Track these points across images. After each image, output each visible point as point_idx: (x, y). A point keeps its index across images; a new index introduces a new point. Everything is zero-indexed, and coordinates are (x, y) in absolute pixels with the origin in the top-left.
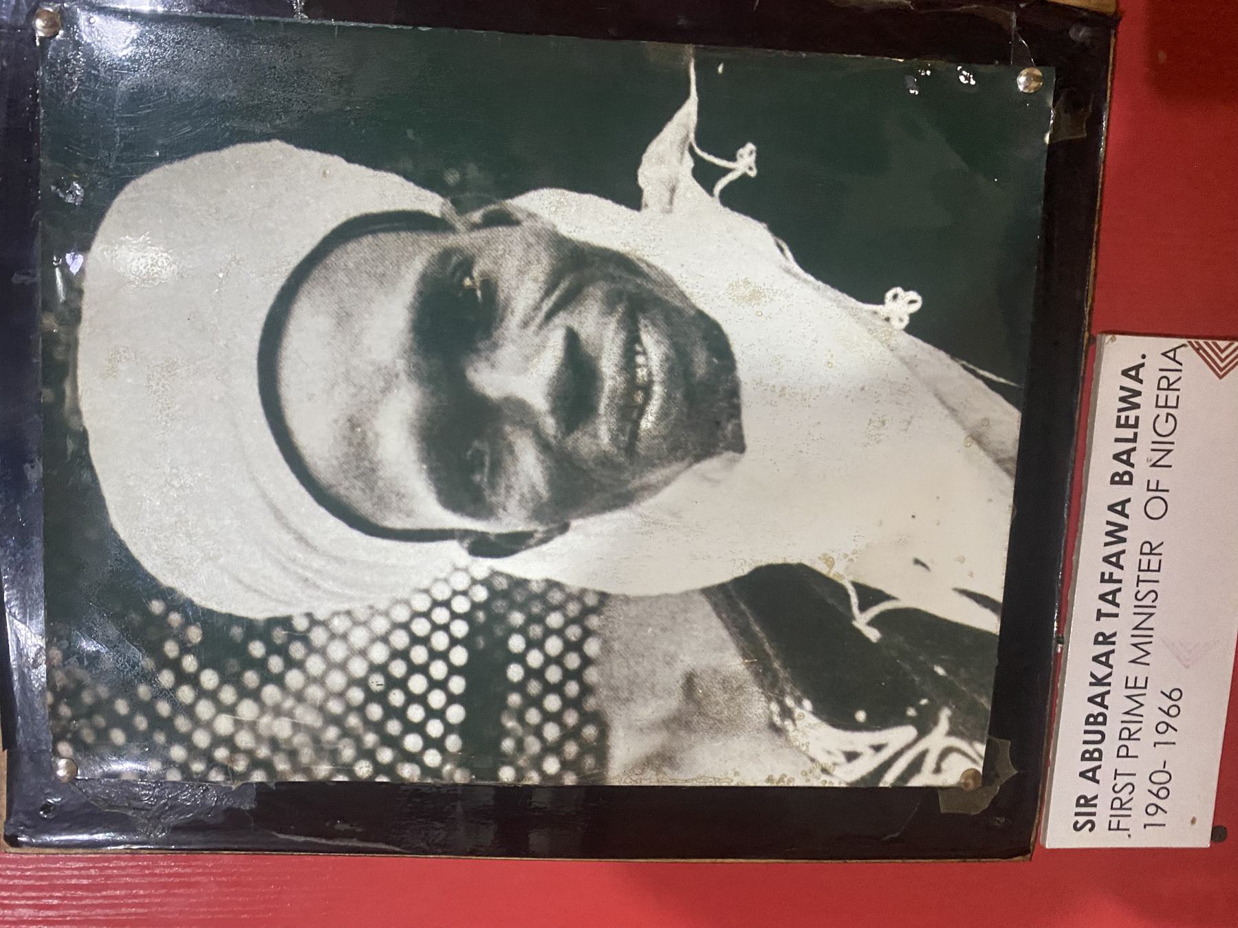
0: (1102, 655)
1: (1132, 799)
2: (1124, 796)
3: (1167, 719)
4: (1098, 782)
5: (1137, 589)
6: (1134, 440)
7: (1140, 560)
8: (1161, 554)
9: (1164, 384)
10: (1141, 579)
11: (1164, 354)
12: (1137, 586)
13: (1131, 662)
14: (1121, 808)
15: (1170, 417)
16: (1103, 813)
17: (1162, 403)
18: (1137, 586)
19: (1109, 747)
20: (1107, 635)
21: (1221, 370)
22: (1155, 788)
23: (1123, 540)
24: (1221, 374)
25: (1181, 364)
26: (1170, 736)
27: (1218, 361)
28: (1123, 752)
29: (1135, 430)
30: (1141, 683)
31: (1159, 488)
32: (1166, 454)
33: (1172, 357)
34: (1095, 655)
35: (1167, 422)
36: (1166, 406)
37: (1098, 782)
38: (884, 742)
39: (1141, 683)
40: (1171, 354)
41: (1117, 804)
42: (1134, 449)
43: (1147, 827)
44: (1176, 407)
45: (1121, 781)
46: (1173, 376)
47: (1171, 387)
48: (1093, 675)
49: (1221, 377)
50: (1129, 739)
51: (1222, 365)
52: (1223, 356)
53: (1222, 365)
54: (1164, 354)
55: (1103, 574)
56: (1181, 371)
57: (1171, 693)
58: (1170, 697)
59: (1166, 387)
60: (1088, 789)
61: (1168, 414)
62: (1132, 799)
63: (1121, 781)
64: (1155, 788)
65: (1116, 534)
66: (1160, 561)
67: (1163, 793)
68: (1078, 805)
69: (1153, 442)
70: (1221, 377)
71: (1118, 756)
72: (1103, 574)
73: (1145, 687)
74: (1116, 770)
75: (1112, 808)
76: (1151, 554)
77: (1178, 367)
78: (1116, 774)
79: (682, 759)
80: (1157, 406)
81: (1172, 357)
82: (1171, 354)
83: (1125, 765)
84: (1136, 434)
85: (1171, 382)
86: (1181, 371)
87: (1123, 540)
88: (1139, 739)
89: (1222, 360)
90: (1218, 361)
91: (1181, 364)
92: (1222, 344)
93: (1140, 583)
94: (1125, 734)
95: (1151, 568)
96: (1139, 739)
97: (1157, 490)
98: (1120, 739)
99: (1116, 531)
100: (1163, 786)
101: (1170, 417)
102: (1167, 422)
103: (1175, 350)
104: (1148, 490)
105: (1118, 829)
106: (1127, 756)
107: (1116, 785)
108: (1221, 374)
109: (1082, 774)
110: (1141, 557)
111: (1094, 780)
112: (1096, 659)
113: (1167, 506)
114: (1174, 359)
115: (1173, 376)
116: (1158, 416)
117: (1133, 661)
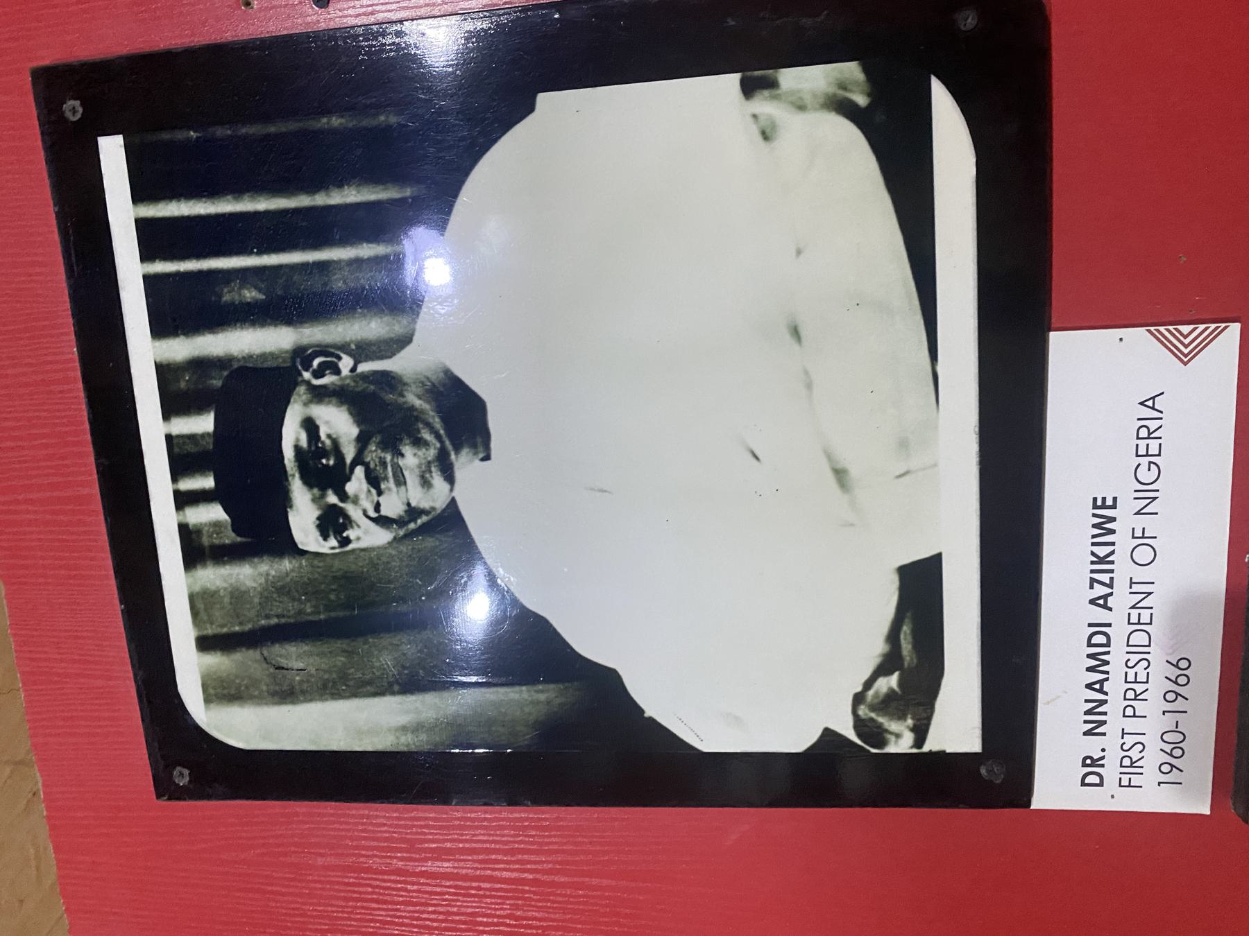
0: (1095, 683)
1: (1143, 757)
2: (1135, 754)
3: (1175, 688)
4: (1110, 609)
5: (1123, 741)
6: (1108, 645)
7: (1137, 445)
8: (1160, 438)
9: (1144, 432)
10: (1133, 581)
11: (1142, 404)
12: (1123, 738)
13: (1135, 514)
14: (1131, 766)
15: (1152, 465)
16: (1111, 771)
17: (1142, 451)
18: (1123, 738)
19: (1114, 706)
20: (1095, 758)
21: (1186, 356)
22: (1168, 748)
23: (1112, 532)
24: (1186, 360)
25: (1161, 412)
26: (1180, 704)
27: (1181, 338)
28: (1129, 712)
29: (1111, 575)
30: (1109, 502)
31: (1141, 622)
32: (1153, 501)
33: (1151, 405)
34: (1092, 598)
35: (1149, 470)
36: (1147, 455)
37: (1110, 609)
38: (803, 340)
39: (1109, 502)
40: (1150, 403)
41: (1127, 762)
42: (1111, 594)
43: (1161, 785)
44: (1151, 624)
45: (1129, 740)
46: (1153, 425)
47: (1134, 765)
48: (1093, 554)
49: (1185, 364)
50: (1135, 699)
51: (1186, 351)
52: (1186, 341)
53: (1186, 351)
54: (1142, 404)
55: (1095, 500)
56: (1161, 419)
57: (1177, 663)
58: (1177, 666)
59: (1146, 436)
60: (1093, 747)
61: (1150, 463)
62: (1143, 757)
63: (1129, 740)
64: (1168, 748)
65: (1098, 663)
66: (1152, 614)
67: (1178, 752)
68: (1084, 765)
69: (1135, 491)
70: (1185, 364)
71: (1124, 716)
72: (1095, 500)
73: (1149, 646)
74: (1123, 729)
75: (1121, 766)
76: (1148, 438)
77: (1159, 415)
78: (1123, 733)
79: (363, 248)
80: (1137, 455)
81: (1151, 405)
82: (1150, 403)
83: (1131, 724)
84: (1112, 579)
85: (1151, 431)
86: (1161, 419)
87: (1112, 532)
88: (1104, 734)
89: (1186, 346)
90: (1181, 338)
91: (1161, 412)
92: (1185, 329)
93: (1133, 585)
94: (1131, 695)
95: (1137, 714)
96: (1104, 734)
97: (1143, 537)
98: (1125, 699)
99: (1103, 523)
100: (1176, 745)
101: (1152, 465)
102: (1149, 470)
103: (1153, 398)
104: (1133, 537)
105: (1129, 786)
106: (1134, 716)
107: (1124, 743)
108: (1186, 360)
109: (1093, 602)
110: (1139, 442)
111: (1105, 606)
112: (1089, 686)
113: (1155, 555)
114: (1153, 408)
115: (1153, 425)
116: (1139, 465)
117: (1138, 513)
